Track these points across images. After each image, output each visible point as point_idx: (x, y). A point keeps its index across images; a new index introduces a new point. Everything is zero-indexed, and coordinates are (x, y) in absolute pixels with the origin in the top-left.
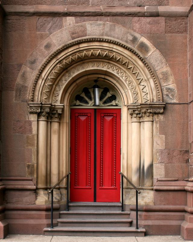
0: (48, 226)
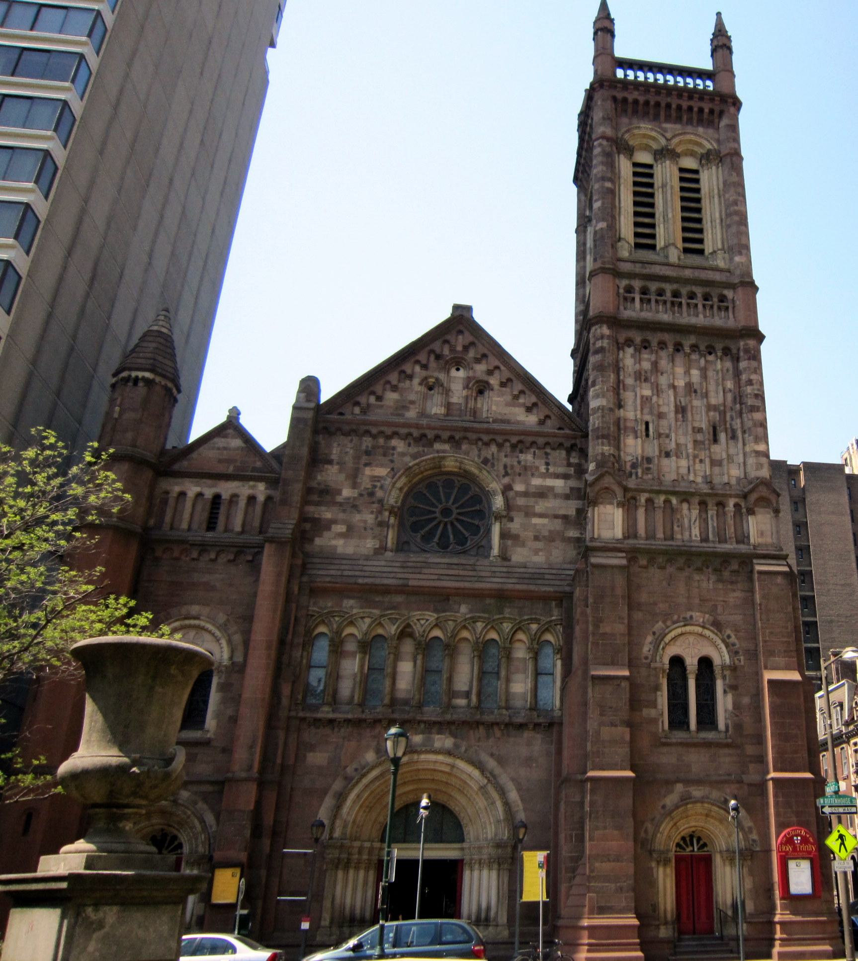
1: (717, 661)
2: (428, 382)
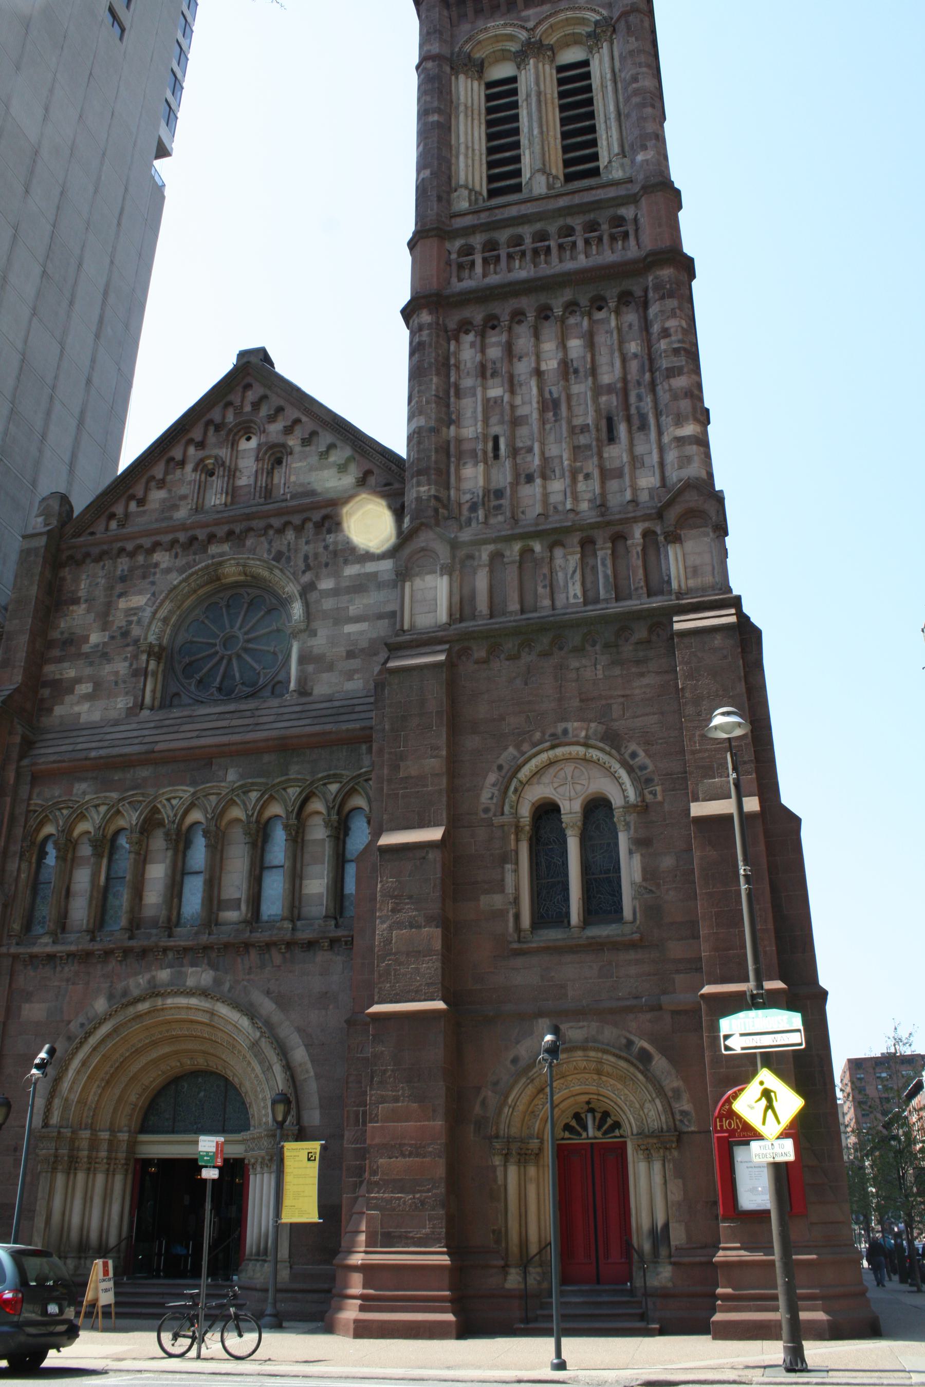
0: (522, 1321)
1: (617, 801)
2: (206, 466)
